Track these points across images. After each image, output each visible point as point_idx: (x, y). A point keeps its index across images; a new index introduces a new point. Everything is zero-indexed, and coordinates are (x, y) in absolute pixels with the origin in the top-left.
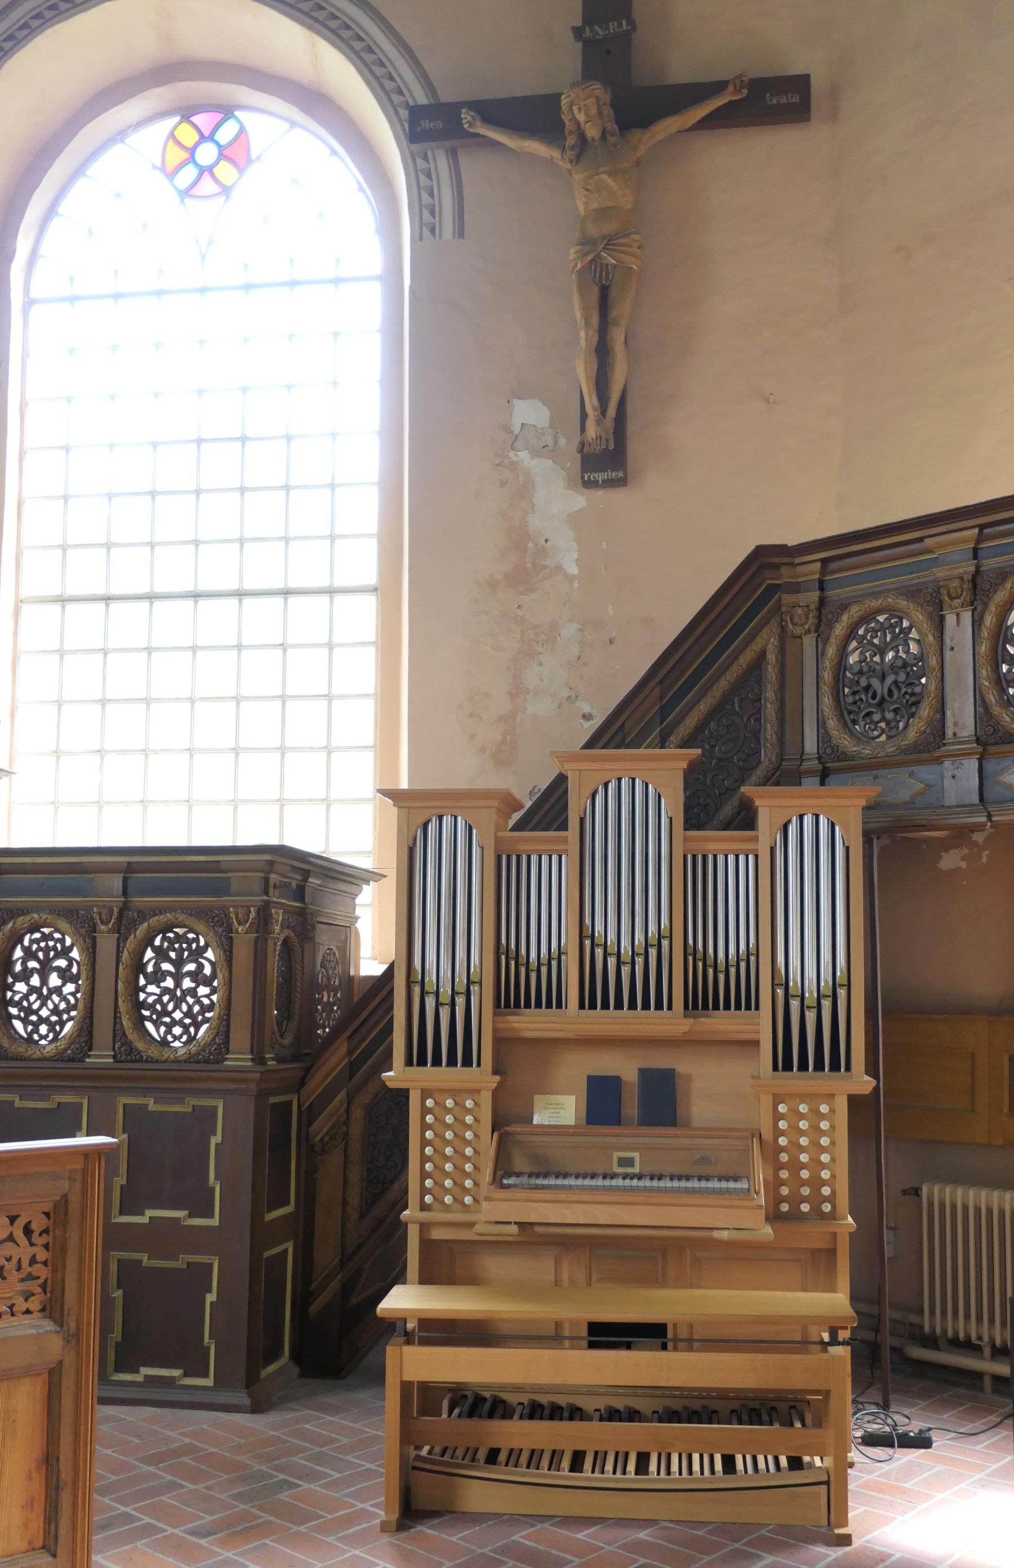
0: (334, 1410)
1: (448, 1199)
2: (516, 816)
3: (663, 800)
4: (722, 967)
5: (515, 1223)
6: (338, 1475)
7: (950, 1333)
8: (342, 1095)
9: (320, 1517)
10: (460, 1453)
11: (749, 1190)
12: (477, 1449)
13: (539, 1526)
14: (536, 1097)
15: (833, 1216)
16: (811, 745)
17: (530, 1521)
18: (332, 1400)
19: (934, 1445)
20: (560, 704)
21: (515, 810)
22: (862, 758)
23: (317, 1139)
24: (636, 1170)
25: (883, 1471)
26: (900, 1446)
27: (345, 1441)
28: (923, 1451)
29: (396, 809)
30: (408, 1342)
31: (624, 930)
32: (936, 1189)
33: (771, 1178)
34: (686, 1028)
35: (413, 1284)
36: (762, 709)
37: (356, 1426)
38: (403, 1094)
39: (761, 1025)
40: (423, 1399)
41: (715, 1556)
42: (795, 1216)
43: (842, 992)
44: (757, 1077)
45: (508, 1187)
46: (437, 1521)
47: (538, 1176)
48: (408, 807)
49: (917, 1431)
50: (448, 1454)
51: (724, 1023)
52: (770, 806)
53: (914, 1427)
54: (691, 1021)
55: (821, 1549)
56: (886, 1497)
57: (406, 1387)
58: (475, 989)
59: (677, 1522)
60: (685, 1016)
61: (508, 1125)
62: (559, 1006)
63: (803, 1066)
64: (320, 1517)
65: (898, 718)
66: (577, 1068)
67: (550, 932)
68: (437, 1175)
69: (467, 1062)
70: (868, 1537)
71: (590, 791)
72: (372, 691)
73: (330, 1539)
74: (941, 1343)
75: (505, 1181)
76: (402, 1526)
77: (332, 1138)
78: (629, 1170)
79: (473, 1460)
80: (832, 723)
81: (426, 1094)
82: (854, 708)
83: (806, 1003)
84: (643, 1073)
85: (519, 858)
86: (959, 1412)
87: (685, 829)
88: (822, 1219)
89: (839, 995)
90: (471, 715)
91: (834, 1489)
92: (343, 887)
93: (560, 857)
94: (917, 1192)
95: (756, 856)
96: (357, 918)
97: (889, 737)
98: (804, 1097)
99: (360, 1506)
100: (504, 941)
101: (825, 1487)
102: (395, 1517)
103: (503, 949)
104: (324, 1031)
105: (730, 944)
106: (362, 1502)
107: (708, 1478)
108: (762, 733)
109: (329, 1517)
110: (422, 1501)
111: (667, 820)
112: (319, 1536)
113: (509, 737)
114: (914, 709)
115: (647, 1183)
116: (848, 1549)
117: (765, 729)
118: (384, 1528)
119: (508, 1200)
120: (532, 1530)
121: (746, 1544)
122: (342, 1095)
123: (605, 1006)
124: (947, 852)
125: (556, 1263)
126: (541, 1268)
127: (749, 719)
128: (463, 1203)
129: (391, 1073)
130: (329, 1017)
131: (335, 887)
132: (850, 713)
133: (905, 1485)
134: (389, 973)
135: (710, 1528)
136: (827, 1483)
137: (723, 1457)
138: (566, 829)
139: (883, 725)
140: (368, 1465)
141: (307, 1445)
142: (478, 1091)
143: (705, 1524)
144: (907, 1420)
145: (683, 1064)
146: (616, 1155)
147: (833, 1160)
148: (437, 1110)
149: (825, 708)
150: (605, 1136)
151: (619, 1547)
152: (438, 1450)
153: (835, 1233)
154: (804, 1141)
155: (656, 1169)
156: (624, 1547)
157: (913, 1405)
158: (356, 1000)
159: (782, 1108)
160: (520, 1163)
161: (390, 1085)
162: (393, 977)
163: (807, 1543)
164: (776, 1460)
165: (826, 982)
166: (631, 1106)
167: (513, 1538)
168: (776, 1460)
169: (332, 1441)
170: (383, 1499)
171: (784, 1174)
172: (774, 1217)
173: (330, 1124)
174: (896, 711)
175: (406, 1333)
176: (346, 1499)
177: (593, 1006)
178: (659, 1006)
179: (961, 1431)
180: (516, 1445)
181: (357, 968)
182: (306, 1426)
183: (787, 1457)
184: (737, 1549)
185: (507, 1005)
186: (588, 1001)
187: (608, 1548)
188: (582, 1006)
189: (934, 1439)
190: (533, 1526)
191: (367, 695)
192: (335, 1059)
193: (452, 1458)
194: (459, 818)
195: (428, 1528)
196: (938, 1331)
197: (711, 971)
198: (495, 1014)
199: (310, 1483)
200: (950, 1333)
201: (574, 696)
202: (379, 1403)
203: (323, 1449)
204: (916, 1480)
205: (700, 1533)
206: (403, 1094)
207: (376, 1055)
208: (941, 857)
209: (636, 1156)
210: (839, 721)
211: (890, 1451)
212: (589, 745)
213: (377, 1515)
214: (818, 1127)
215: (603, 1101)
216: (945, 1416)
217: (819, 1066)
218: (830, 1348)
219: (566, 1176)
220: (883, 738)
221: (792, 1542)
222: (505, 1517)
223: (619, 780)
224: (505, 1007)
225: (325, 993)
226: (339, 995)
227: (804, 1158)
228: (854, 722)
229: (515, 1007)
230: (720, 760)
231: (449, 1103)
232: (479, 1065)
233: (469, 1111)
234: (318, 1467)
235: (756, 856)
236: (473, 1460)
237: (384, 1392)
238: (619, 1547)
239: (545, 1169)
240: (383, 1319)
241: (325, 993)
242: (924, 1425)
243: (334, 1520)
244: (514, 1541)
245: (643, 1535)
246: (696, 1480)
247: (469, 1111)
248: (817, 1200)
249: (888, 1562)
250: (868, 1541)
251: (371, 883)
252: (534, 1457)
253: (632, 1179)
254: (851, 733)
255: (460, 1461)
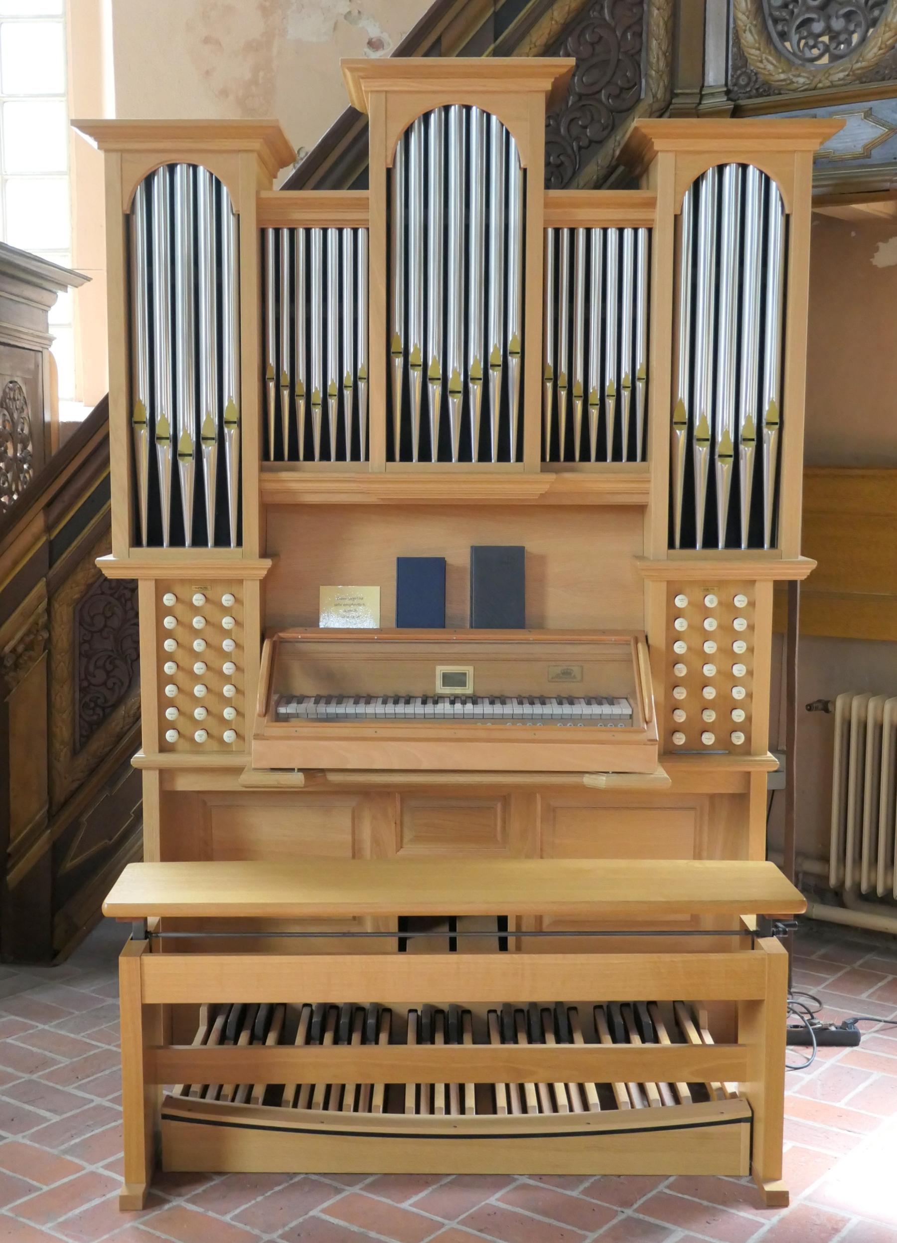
0: (48, 1014)
1: (200, 736)
2: (289, 172)
3: (513, 141)
4: (595, 397)
5: (300, 770)
6: (55, 1118)
7: (864, 887)
8: (40, 587)
9: (31, 1189)
10: (228, 1090)
11: (631, 716)
12: (251, 1087)
13: (349, 1191)
14: (324, 590)
15: (747, 750)
16: (715, 75)
17: (335, 1184)
18: (45, 998)
19: (863, 1039)
20: (336, 24)
21: (283, 164)
22: (794, 91)
23: (7, 649)
24: (468, 690)
25: (804, 1083)
26: (820, 1044)
27: (65, 1061)
28: (848, 1050)
29: (102, 154)
30: (150, 950)
31: (450, 347)
32: (855, 703)
33: (662, 699)
34: (544, 488)
35: (152, 860)
36: (645, 17)
37: (78, 1037)
38: (126, 590)
39: (652, 483)
40: (171, 1024)
41: (601, 1231)
42: (694, 751)
43: (770, 434)
44: (641, 558)
45: (286, 718)
46: (200, 1189)
47: (328, 700)
48: (122, 151)
49: (839, 1024)
50: (212, 1092)
51: (597, 479)
52: (675, 150)
53: (831, 1016)
54: (552, 477)
55: (747, 1214)
56: (816, 1125)
57: (149, 1011)
58: (230, 432)
59: (540, 1177)
60: (543, 470)
61: (283, 629)
62: (356, 457)
63: (710, 541)
64: (31, 1189)
65: (852, 27)
66: (383, 546)
67: (344, 347)
68: (182, 701)
69: (222, 540)
70: (807, 1192)
71: (401, 127)
72: (61, 89)
73: (46, 1228)
74: (848, 897)
75: (282, 710)
76: (151, 1201)
77: (30, 647)
78: (458, 690)
79: (248, 1100)
80: (749, 38)
81: (162, 587)
82: (784, 14)
83: (718, 450)
84: (480, 555)
85: (292, 232)
86: (881, 988)
87: (548, 186)
88: (730, 753)
89: (765, 438)
90: (207, 40)
91: (760, 1126)
92: (29, 292)
93: (355, 231)
94: (826, 707)
95: (650, 231)
96: (51, 340)
97: (834, 58)
98: (707, 587)
99: (90, 1168)
100: (272, 360)
101: (748, 1125)
102: (140, 1188)
103: (271, 372)
104: (11, 498)
105: (606, 367)
106: (92, 1162)
107: (579, 1116)
108: (643, 54)
109: (46, 1188)
110: (176, 1162)
111: (520, 174)
112: (32, 1224)
113: (261, 74)
114: (876, 13)
115: (486, 709)
116: (784, 1212)
117: (648, 49)
118: (125, 1204)
119: (288, 738)
120: (339, 1197)
121: (644, 1209)
122: (40, 587)
123: (425, 456)
124: (885, 240)
125: (353, 819)
126: (333, 827)
127: (624, 34)
128: (221, 741)
129: (109, 558)
130: (16, 478)
131: (15, 290)
132: (776, 21)
133: (838, 1105)
134: (101, 412)
135: (587, 1184)
136: (751, 1120)
137: (599, 1086)
138: (366, 187)
139: (825, 39)
140: (98, 1101)
141: (10, 1070)
142: (240, 582)
143: (581, 1178)
144: (817, 1004)
145: (535, 540)
146: (441, 669)
147: (750, 673)
148: (180, 610)
149: (740, 15)
150: (423, 642)
151: (463, 1222)
152: (196, 1088)
153: (749, 773)
154: (710, 647)
155: (495, 688)
156: (470, 1221)
157: (818, 982)
158: (54, 452)
159: (680, 602)
160: (302, 684)
161: (109, 574)
162: (107, 419)
163: (725, 1203)
164: (673, 1088)
165: (748, 418)
166: (460, 599)
167: (311, 1213)
168: (673, 1088)
169: (45, 1063)
170: (122, 1155)
171: (680, 694)
172: (669, 753)
173: (24, 629)
174: (848, 16)
175: (147, 935)
176: (69, 1158)
177: (406, 456)
178: (504, 456)
179: (888, 1019)
180: (307, 1080)
181: (54, 411)
182: (9, 1040)
183: (690, 1085)
184: (629, 1219)
185: (279, 456)
186: (400, 450)
187: (450, 1224)
188: (390, 457)
189: (861, 1031)
190: (338, 1191)
191: (61, 173)
192: (26, 538)
193: (218, 1098)
194: (201, 169)
195: (192, 1201)
196: (848, 883)
197: (578, 405)
198: (262, 469)
199: (15, 1134)
200: (864, 887)
201: (355, 13)
202: (110, 1001)
203: (34, 1077)
204: (850, 1096)
205: (574, 1194)
206: (126, 590)
207: (75, 544)
208: (877, 249)
209: (469, 670)
210: (760, 33)
211: (807, 1052)
212: (406, 50)
213: (115, 1184)
214: (728, 627)
215: (419, 593)
216: (864, 996)
217: (733, 541)
218: (762, 942)
219: (369, 699)
220: (825, 60)
221: (705, 1203)
222: (297, 1179)
223: (447, 109)
224: (276, 459)
225: (9, 445)
226: (30, 448)
227: (709, 670)
228: (783, 36)
229: (290, 459)
230: (580, 96)
231: (198, 600)
232: (239, 543)
233: (226, 611)
234: (27, 1107)
235: (650, 231)
236: (248, 1100)
237: (117, 983)
238: (463, 1222)
239: (338, 690)
240: (113, 919)
241: (9, 445)
242: (849, 1013)
243: (51, 1193)
244: (313, 1217)
245: (495, 1200)
246: (564, 1120)
247: (226, 611)
248: (726, 728)
249: (844, 1233)
250: (809, 1198)
251: (70, 289)
252: (333, 1096)
253: (464, 703)
254: (779, 54)
255: (229, 1103)
